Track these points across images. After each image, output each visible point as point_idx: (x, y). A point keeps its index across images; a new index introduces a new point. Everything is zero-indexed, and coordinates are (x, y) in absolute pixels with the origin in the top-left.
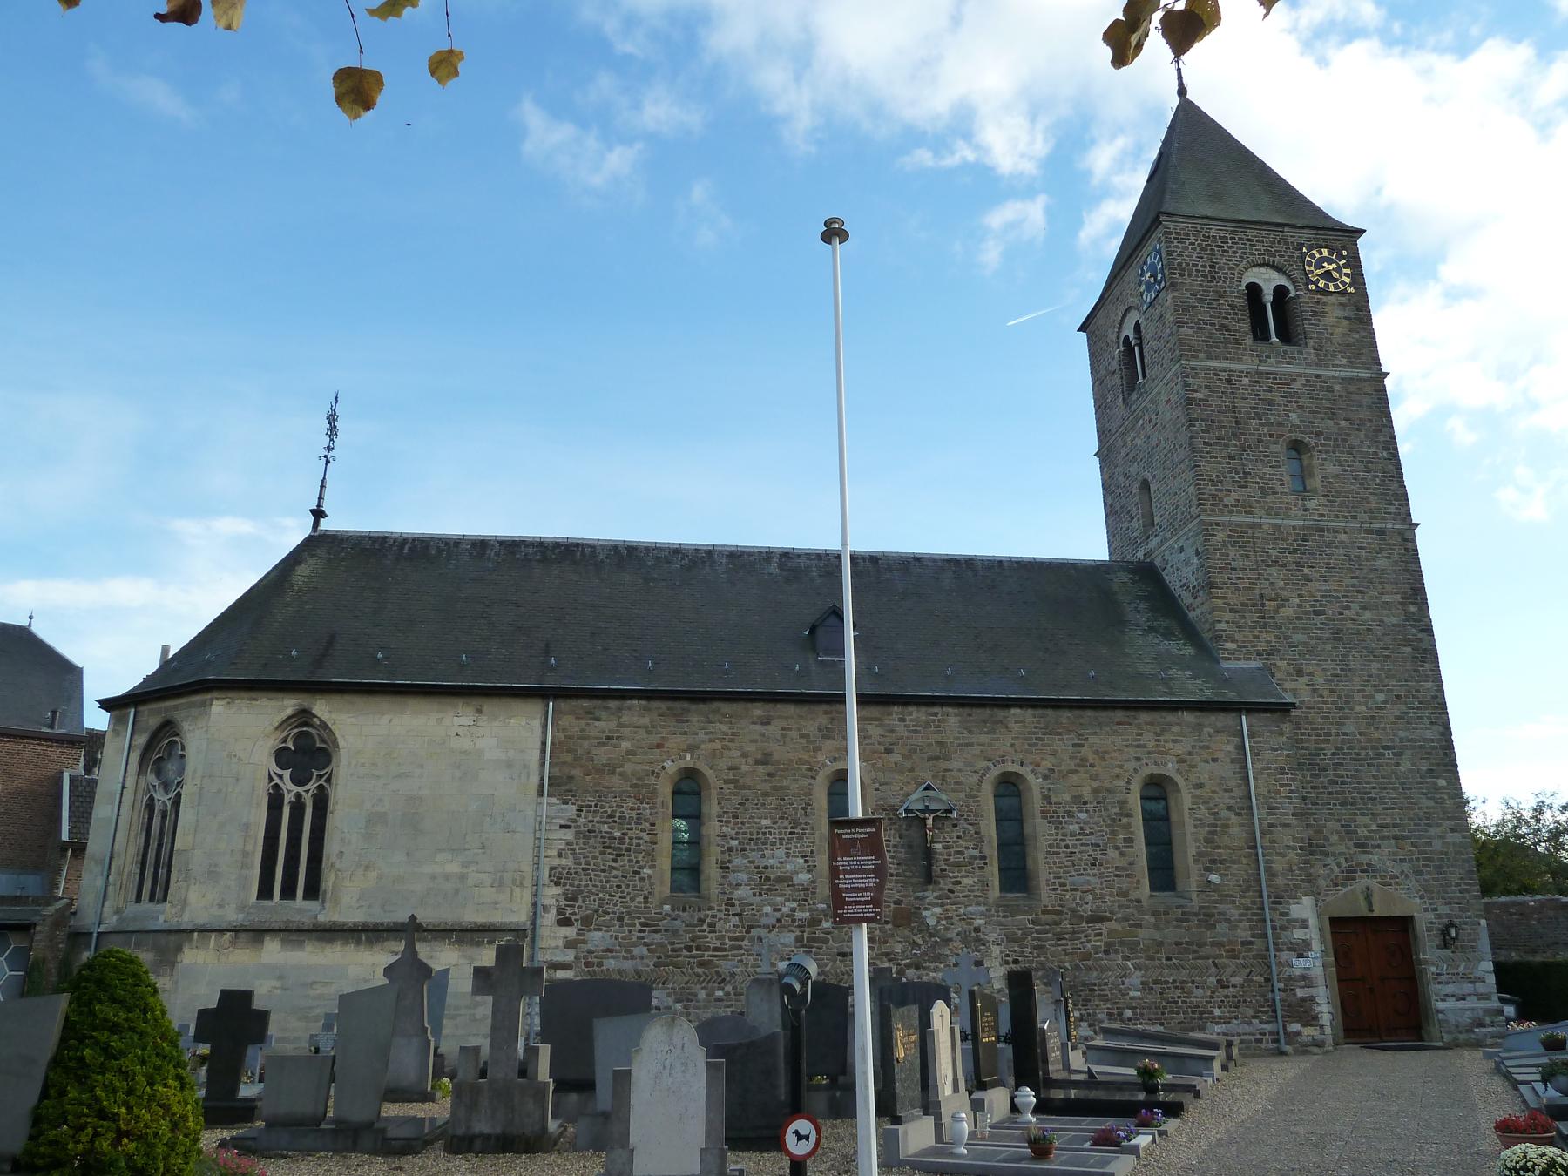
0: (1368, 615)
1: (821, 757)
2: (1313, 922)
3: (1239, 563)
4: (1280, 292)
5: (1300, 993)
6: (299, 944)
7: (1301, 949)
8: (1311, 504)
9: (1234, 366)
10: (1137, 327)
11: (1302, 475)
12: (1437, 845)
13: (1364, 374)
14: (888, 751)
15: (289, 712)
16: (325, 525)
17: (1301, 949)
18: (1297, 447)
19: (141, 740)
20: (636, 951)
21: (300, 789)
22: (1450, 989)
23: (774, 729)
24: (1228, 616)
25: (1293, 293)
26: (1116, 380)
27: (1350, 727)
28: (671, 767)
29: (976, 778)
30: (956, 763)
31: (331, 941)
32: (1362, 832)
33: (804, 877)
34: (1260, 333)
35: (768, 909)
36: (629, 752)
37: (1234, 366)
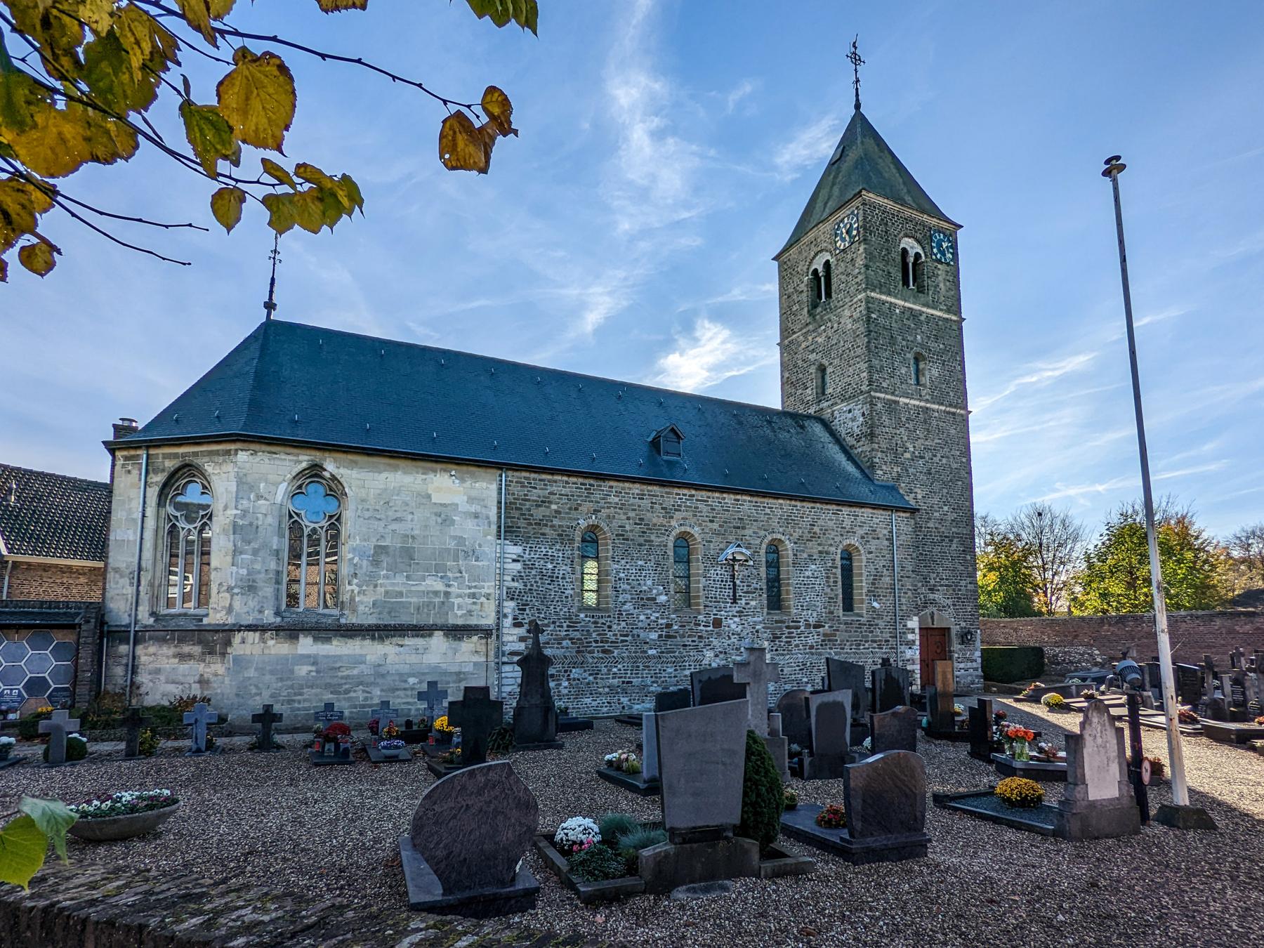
0: (944, 461)
1: (673, 523)
3: (887, 423)
4: (917, 256)
6: (328, 640)
7: (910, 644)
8: (923, 393)
9: (893, 300)
10: (827, 264)
13: (954, 318)
14: (712, 521)
15: (304, 465)
17: (910, 644)
19: (159, 478)
20: (564, 643)
22: (962, 665)
23: (646, 503)
24: (879, 455)
25: (923, 258)
26: (804, 297)
27: (931, 525)
28: (583, 524)
29: (758, 542)
30: (748, 532)
31: (351, 637)
32: (932, 582)
33: (663, 598)
35: (642, 617)
36: (556, 511)
37: (893, 300)
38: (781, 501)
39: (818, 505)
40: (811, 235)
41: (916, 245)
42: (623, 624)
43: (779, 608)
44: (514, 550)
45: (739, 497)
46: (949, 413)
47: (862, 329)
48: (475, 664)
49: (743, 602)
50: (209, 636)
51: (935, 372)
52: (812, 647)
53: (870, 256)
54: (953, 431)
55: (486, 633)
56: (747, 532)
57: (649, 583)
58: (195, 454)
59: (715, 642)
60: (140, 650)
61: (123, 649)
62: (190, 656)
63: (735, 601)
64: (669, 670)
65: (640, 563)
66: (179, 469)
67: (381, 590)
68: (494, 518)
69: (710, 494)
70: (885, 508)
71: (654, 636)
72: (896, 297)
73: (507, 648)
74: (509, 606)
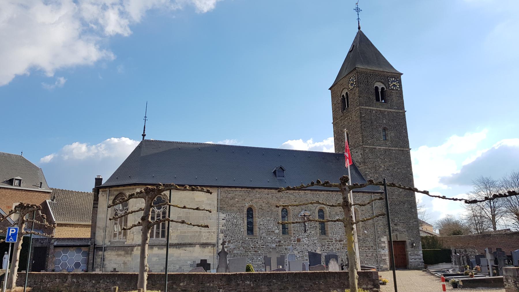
0: (399, 170)
2: (386, 242)
4: (383, 89)
5: (383, 258)
7: (383, 248)
8: (387, 143)
9: (371, 108)
11: (385, 136)
12: (412, 224)
16: (146, 138)
17: (383, 248)
18: (385, 129)
19: (112, 198)
21: (159, 211)
22: (413, 257)
23: (270, 196)
24: (368, 170)
28: (247, 205)
32: (396, 221)
33: (277, 231)
34: (378, 100)
35: (269, 239)
37: (371, 108)
40: (341, 82)
41: (382, 84)
42: (262, 241)
43: (325, 234)
44: (222, 216)
46: (400, 150)
47: (359, 121)
48: (210, 256)
49: (309, 232)
50: (126, 248)
51: (393, 134)
52: (338, 249)
53: (360, 92)
54: (402, 158)
55: (213, 245)
57: (272, 225)
58: (124, 190)
59: (298, 248)
60: (106, 253)
61: (100, 253)
62: (121, 255)
63: (305, 232)
66: (118, 195)
67: (179, 231)
68: (216, 205)
70: (368, 192)
72: (373, 107)
74: (221, 236)
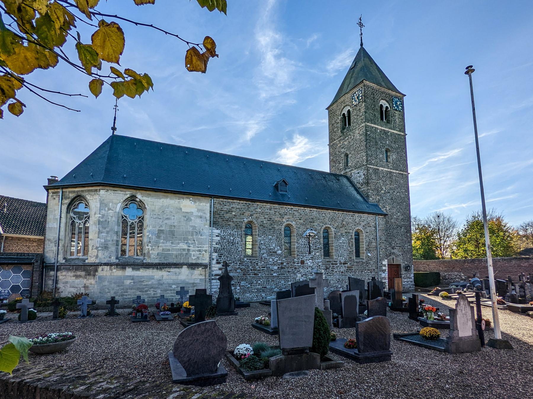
0: (398, 194)
1: (284, 220)
3: (374, 178)
4: (387, 108)
6: (138, 269)
7: (384, 271)
8: (389, 165)
9: (377, 126)
10: (349, 111)
13: (402, 134)
14: (300, 219)
15: (128, 196)
17: (384, 271)
19: (67, 201)
20: (238, 271)
22: (406, 280)
23: (272, 212)
24: (371, 191)
25: (389, 109)
26: (339, 125)
27: (392, 221)
28: (246, 220)
29: (320, 228)
30: (315, 224)
31: (148, 268)
32: (393, 245)
33: (280, 252)
35: (271, 260)
36: (234, 215)
37: (377, 126)
38: (329, 211)
39: (345, 213)
40: (342, 99)
41: (386, 103)
42: (263, 263)
43: (329, 256)
44: (217, 232)
45: (311, 209)
46: (400, 174)
47: (364, 139)
48: (200, 279)
49: (313, 253)
50: (88, 268)
51: (394, 157)
52: (342, 272)
53: (367, 108)
54: (402, 182)
55: (205, 266)
56: (315, 224)
57: (274, 245)
58: (82, 191)
59: (302, 270)
60: (59, 273)
61: (52, 273)
62: (80, 276)
63: (310, 253)
64: (282, 282)
65: (270, 237)
66: (75, 197)
67: (161, 248)
68: (208, 218)
69: (299, 208)
70: (373, 214)
71: (276, 268)
72: (378, 125)
73: (214, 273)
74: (215, 255)
